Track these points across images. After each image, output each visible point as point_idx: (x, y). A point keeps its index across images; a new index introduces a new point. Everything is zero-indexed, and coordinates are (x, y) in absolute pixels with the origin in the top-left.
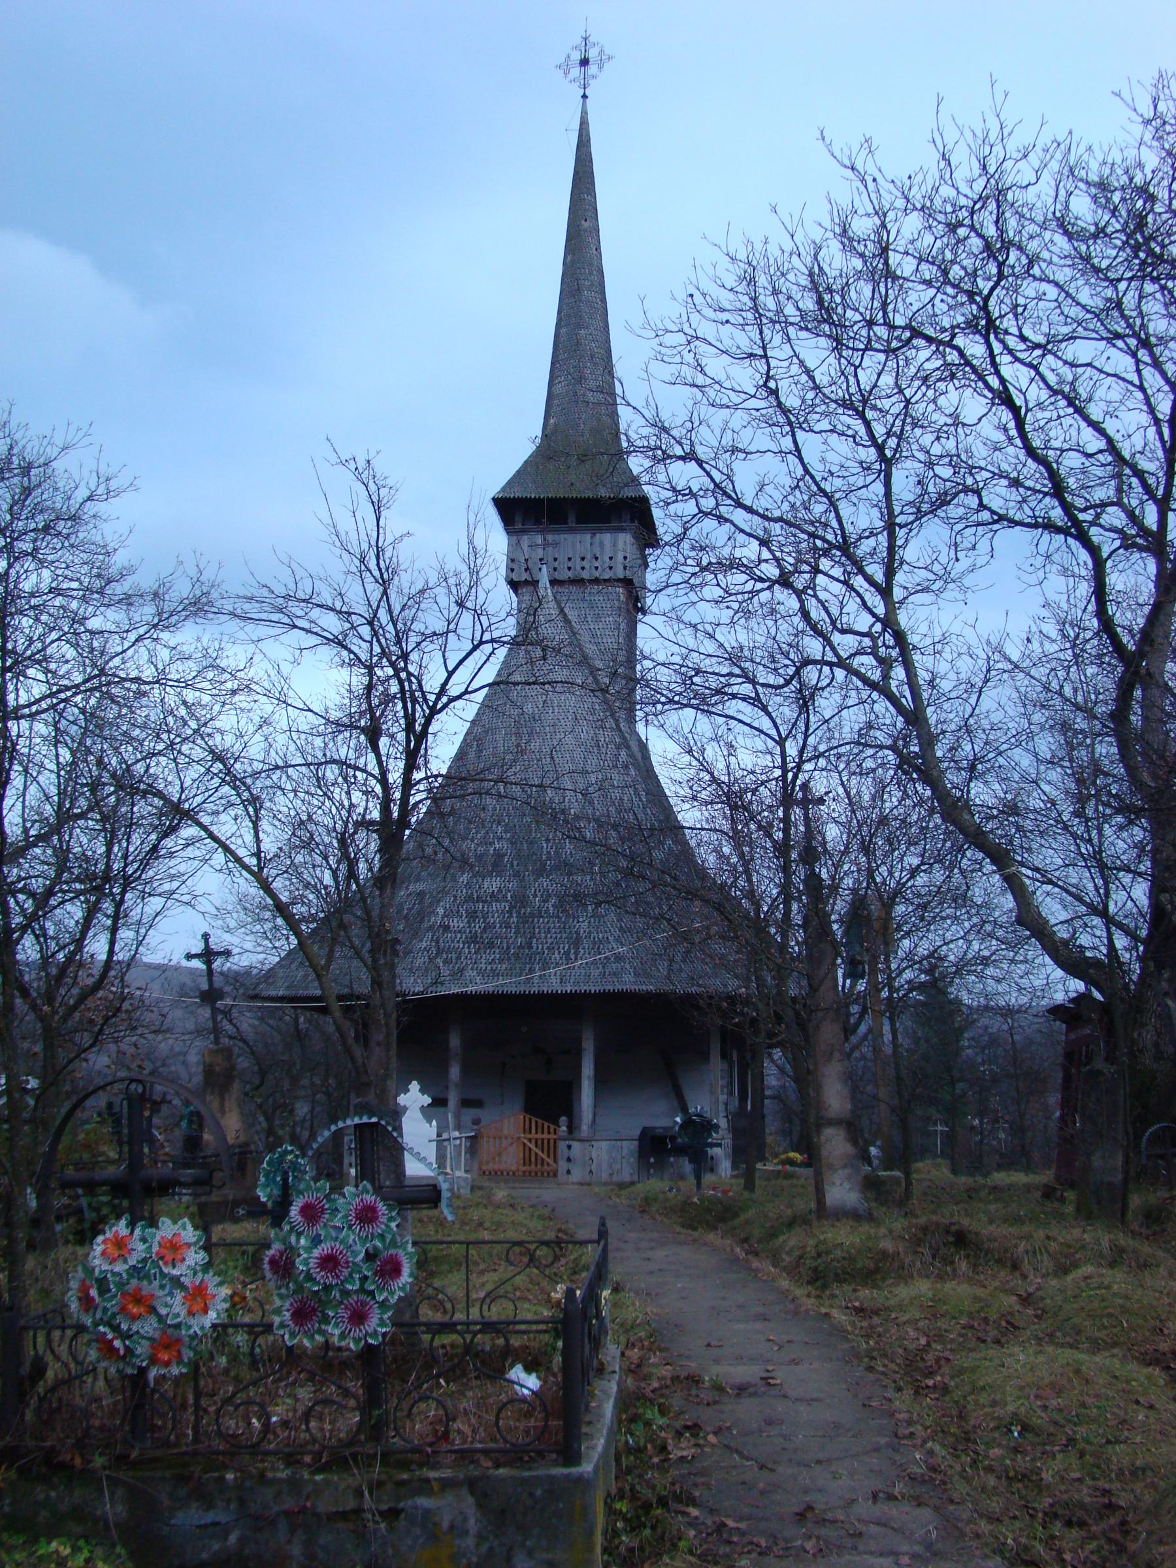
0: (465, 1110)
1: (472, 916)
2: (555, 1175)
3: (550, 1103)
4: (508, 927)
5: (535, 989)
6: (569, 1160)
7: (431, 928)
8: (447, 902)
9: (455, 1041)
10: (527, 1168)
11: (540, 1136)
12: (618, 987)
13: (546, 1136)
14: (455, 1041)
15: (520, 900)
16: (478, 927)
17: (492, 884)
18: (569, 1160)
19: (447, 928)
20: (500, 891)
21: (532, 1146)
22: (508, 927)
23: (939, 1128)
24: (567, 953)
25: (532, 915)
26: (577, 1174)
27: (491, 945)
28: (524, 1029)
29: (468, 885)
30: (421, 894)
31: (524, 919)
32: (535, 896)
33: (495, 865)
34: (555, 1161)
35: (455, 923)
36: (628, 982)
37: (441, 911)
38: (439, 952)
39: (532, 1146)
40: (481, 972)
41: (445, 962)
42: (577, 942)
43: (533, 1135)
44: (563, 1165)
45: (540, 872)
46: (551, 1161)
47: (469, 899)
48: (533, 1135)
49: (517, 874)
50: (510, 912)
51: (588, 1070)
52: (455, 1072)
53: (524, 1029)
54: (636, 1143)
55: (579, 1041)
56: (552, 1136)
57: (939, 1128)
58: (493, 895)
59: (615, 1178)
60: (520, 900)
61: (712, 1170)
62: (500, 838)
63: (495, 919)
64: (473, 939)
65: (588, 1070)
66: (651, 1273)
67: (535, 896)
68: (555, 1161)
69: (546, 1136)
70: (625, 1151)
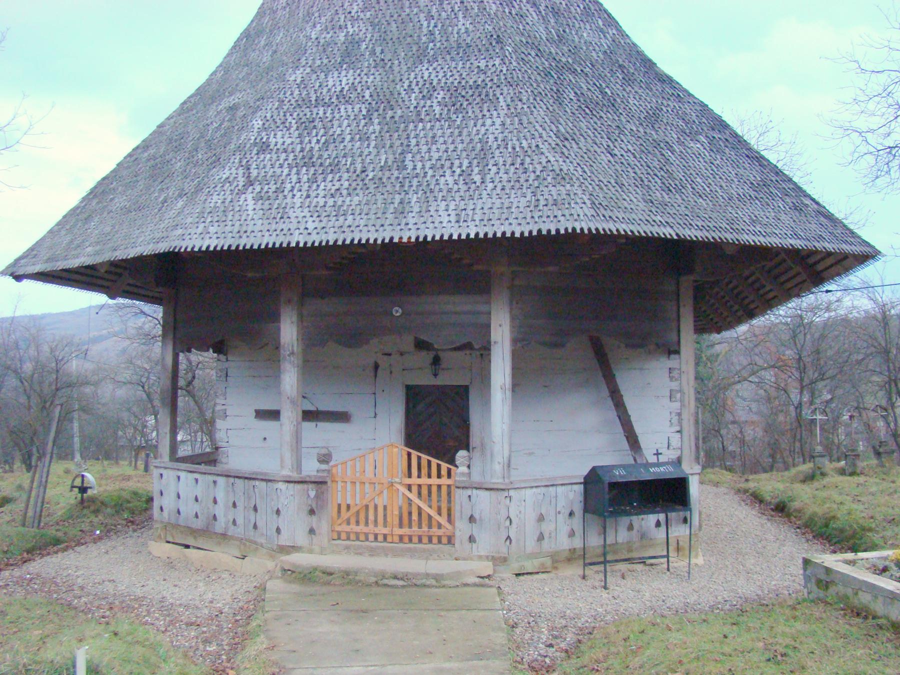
0: (306, 425)
1: (306, 126)
2: (450, 540)
3: (439, 426)
5: (409, 234)
6: (472, 519)
8: (269, 108)
11: (424, 480)
12: (565, 225)
13: (434, 481)
14: (289, 332)
18: (472, 519)
19: (264, 147)
20: (353, 87)
24: (466, 174)
26: (487, 543)
27: (335, 167)
28: (397, 312)
29: (303, 84)
30: (233, 109)
31: (390, 126)
33: (347, 54)
34: (450, 520)
35: (278, 139)
37: (257, 123)
39: (413, 496)
41: (258, 198)
42: (484, 155)
43: (414, 480)
44: (462, 528)
46: (443, 520)
47: (303, 102)
48: (414, 480)
50: (369, 117)
52: (290, 379)
53: (397, 312)
54: (582, 486)
55: (486, 328)
56: (444, 481)
63: (343, 128)
66: (324, 594)
67: (410, 89)
69: (434, 481)
70: (562, 504)
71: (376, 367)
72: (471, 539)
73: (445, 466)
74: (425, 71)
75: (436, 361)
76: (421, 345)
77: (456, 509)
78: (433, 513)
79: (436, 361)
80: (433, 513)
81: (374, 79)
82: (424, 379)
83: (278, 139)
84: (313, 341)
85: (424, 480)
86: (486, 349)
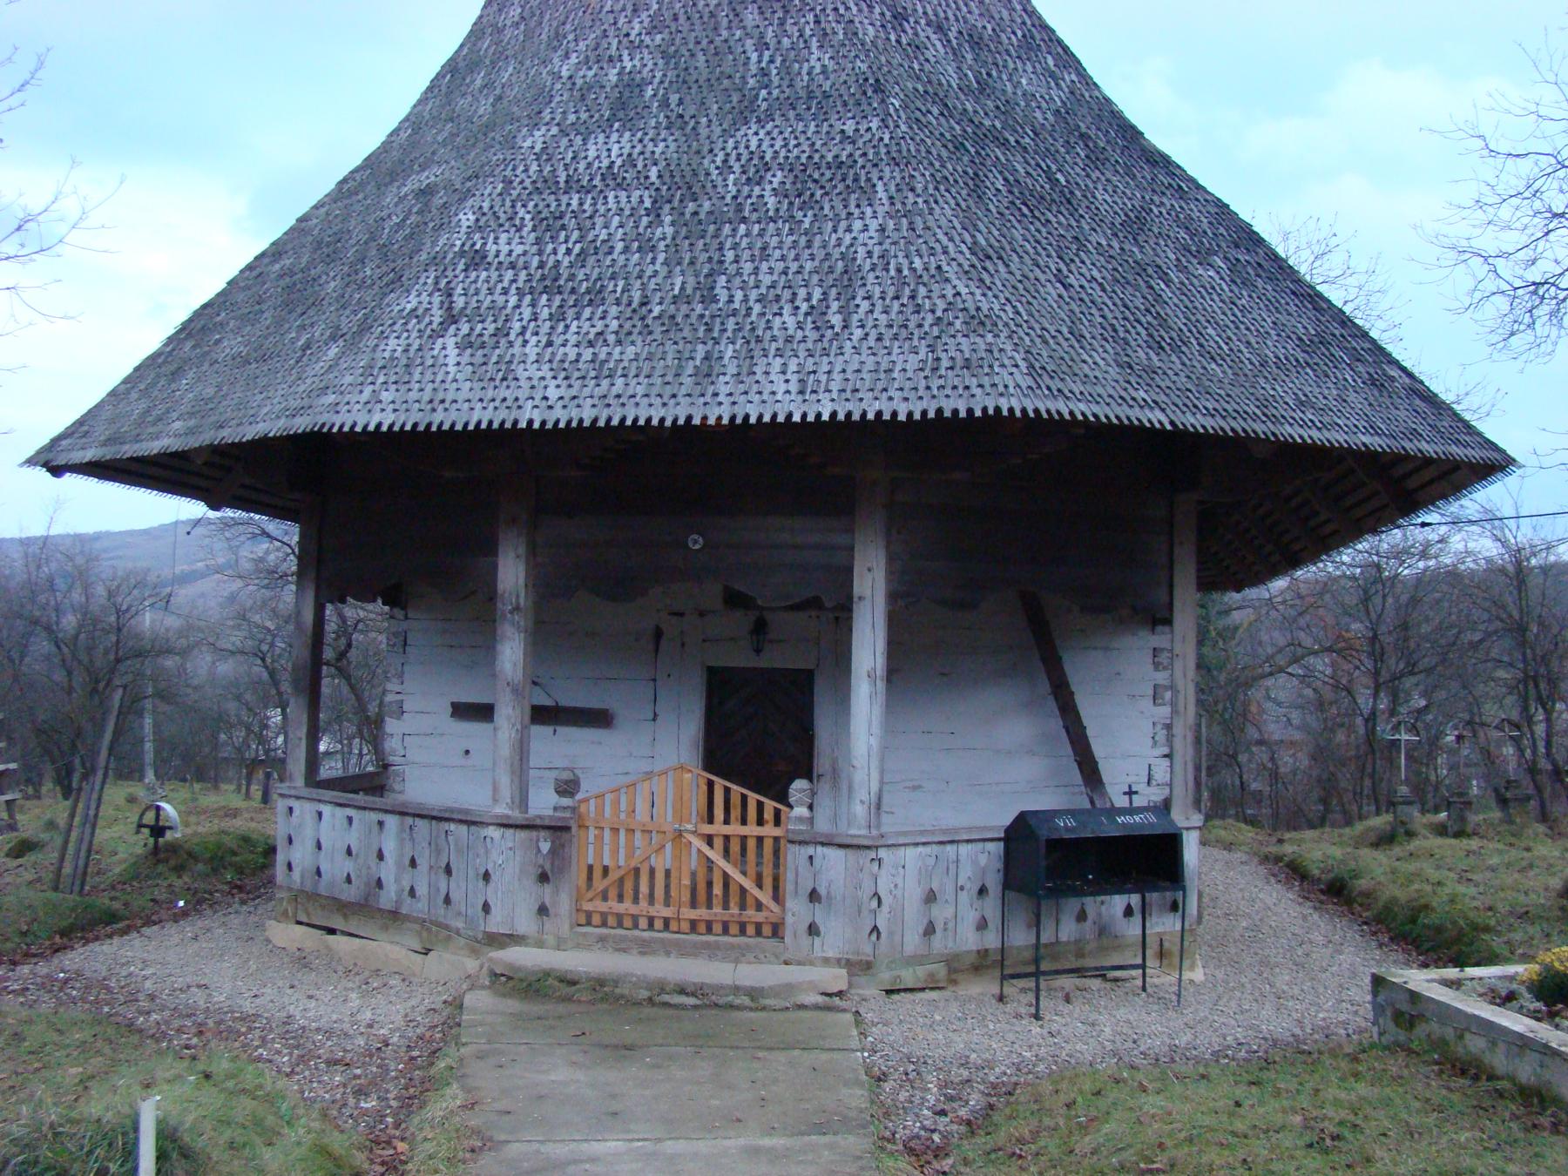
1: (548, 225)
2: (777, 931)
3: (763, 739)
4: (647, 247)
5: (719, 412)
6: (814, 896)
7: (435, 260)
8: (487, 194)
9: (512, 573)
10: (701, 913)
11: (735, 829)
12: (983, 402)
13: (752, 830)
14: (512, 573)
15: (683, 185)
16: (561, 254)
17: (611, 148)
18: (814, 896)
19: (477, 259)
20: (630, 161)
21: (715, 855)
22: (647, 247)
23: (1405, 737)
24: (818, 312)
25: (716, 217)
26: (838, 937)
27: (596, 296)
28: (696, 542)
30: (426, 192)
31: (691, 229)
32: (726, 167)
33: (620, 105)
34: (777, 896)
35: (502, 245)
36: (1009, 391)
37: (467, 218)
38: (451, 318)
39: (715, 855)
40: (564, 371)
41: (465, 345)
42: (847, 280)
43: (718, 828)
44: (797, 911)
45: (745, 112)
46: (765, 897)
47: (546, 184)
48: (718, 828)
49: (677, 122)
50: (655, 213)
51: (869, 647)
52: (511, 653)
53: (696, 542)
55: (844, 575)
56: (769, 830)
57: (1405, 737)
58: (609, 174)
59: (939, 943)
60: (683, 185)
61: (74, 163)
62: (634, 47)
64: (550, 284)
65: (869, 647)
67: (726, 167)
68: (777, 896)
69: (752, 830)
70: (966, 872)
71: (658, 634)
72: (813, 930)
73: (770, 805)
74: (752, 136)
75: (760, 627)
76: (734, 600)
77: (789, 876)
78: (748, 884)
79: (760, 627)
80: (748, 884)
81: (666, 147)
82: (739, 658)
83: (502, 245)
84: (550, 589)
85: (735, 829)
86: (842, 613)
